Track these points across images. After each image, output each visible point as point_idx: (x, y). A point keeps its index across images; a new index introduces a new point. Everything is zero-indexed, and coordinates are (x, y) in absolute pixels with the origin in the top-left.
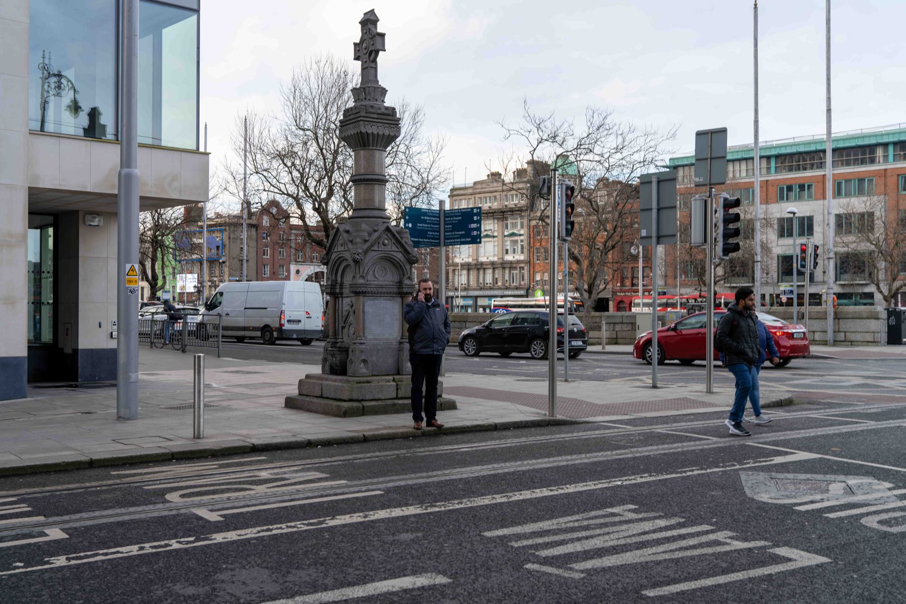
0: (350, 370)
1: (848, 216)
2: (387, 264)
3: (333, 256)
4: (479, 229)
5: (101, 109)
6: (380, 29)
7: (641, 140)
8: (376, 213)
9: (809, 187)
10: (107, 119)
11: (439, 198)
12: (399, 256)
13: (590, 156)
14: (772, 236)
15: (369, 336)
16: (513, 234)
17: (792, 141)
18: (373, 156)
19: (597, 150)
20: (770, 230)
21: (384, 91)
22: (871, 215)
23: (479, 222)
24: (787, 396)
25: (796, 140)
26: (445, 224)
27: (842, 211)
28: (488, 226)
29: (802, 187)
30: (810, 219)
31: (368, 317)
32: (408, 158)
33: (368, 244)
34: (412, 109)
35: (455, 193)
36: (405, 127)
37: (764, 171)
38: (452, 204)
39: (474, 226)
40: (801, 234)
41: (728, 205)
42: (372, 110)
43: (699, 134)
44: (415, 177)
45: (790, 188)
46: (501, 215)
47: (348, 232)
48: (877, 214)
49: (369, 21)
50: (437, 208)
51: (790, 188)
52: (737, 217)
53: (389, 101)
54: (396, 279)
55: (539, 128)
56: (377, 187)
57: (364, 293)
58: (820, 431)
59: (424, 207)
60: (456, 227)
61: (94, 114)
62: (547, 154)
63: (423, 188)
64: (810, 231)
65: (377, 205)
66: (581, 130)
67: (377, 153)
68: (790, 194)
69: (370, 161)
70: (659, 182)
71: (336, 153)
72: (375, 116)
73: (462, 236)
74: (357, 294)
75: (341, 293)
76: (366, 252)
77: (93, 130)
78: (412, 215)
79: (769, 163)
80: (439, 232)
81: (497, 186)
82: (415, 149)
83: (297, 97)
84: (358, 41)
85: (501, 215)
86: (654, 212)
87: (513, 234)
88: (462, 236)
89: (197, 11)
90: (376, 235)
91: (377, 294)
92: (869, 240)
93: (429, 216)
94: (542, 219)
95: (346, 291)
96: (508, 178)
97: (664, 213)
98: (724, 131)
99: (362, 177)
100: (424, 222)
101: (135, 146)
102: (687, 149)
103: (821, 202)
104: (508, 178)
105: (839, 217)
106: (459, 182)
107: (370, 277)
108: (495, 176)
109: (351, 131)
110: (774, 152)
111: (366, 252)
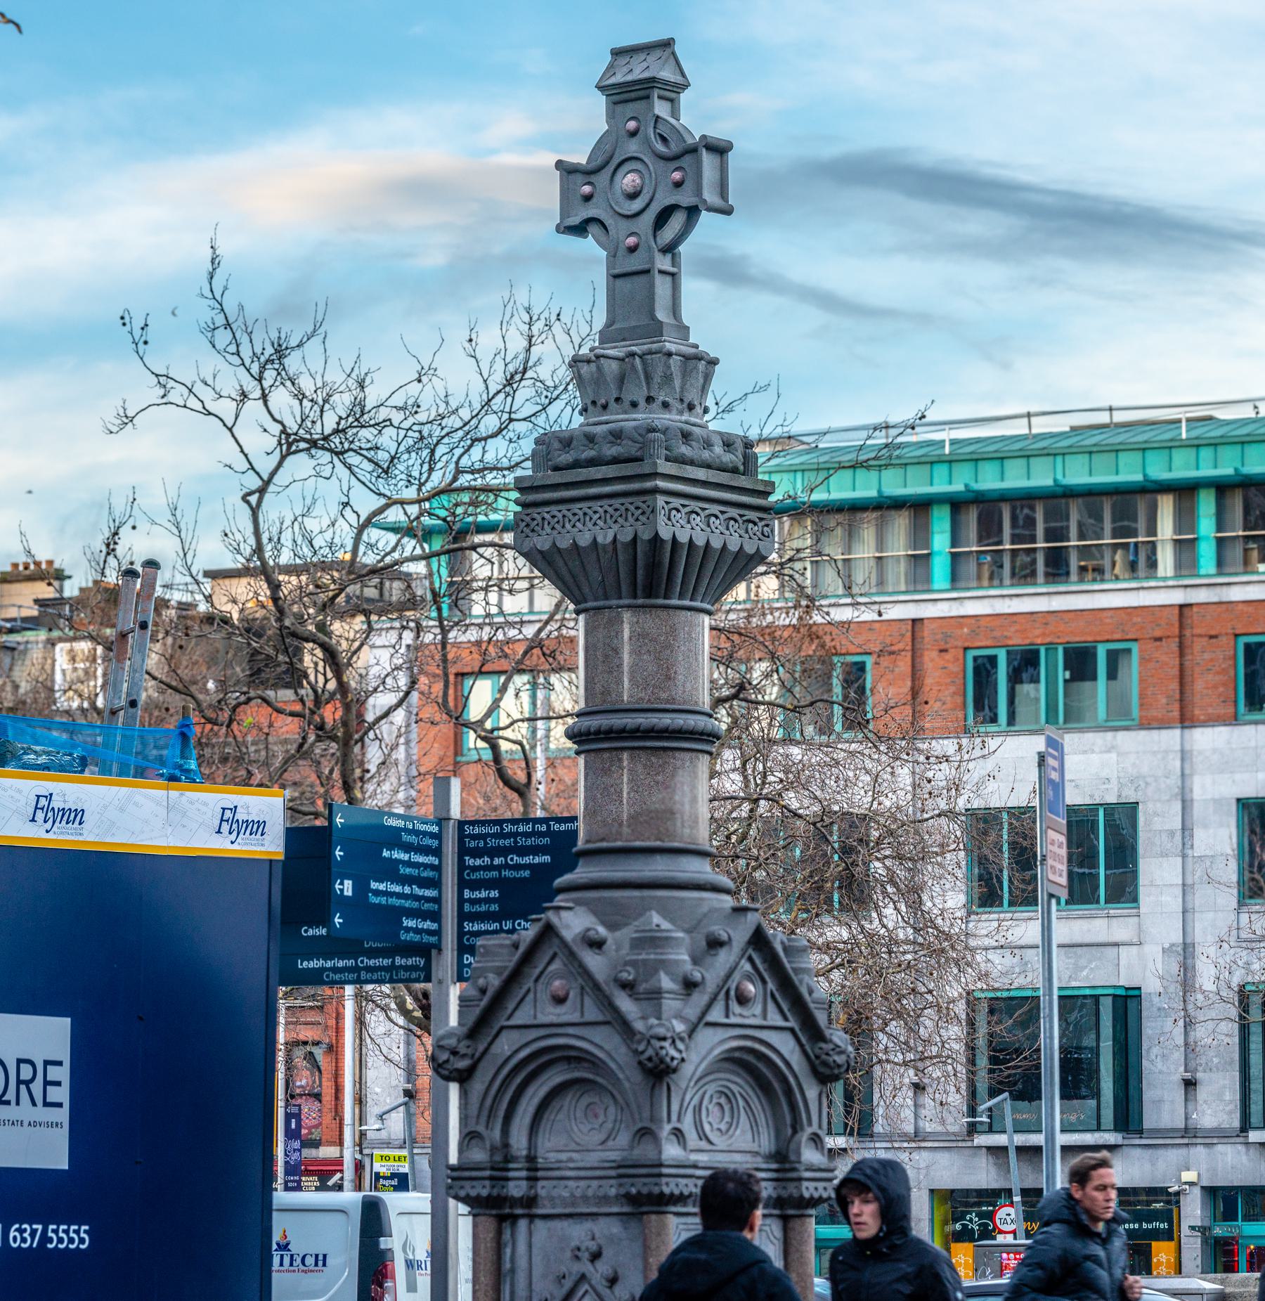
2: (739, 1084)
3: (506, 1045)
9: (1114, 659)
17: (1020, 428)
21: (701, 365)
25: (1041, 426)
26: (463, 884)
29: (1080, 663)
33: (700, 999)
37: (898, 574)
42: (684, 450)
49: (639, 85)
51: (1025, 664)
68: (1025, 689)
72: (701, 474)
75: (531, 1201)
80: (436, 916)
84: (580, 157)
93: (408, 848)
99: (618, 721)
100: (390, 871)
103: (1171, 737)
109: (595, 529)
110: (942, 483)
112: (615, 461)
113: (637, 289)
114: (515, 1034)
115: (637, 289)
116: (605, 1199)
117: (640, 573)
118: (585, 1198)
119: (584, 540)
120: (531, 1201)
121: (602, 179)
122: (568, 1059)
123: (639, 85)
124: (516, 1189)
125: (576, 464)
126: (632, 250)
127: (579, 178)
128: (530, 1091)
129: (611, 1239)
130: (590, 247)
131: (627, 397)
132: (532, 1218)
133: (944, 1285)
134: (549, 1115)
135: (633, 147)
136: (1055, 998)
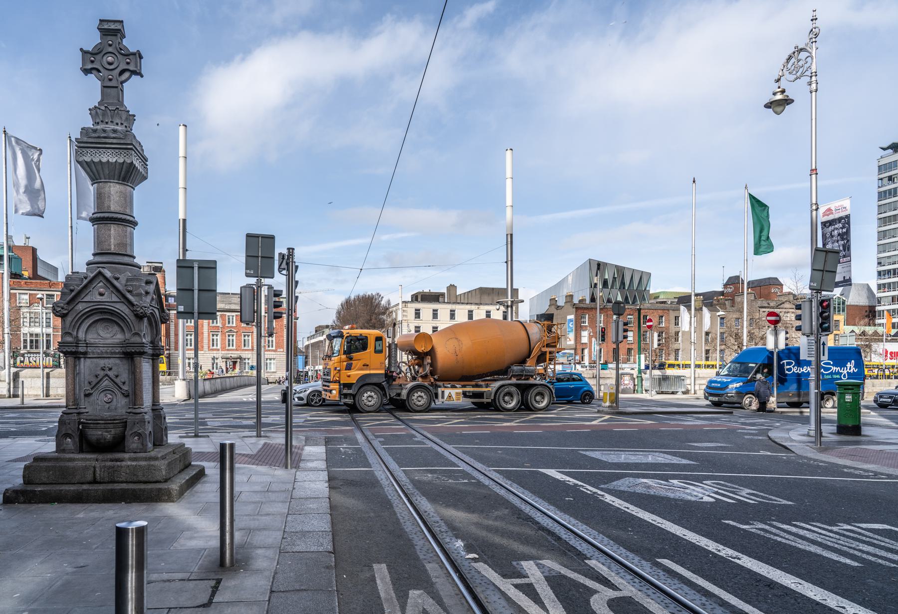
3: (80, 307)
8: (126, 260)
49: (111, 31)
86: (196, 292)
99: (111, 215)
112: (114, 138)
113: (112, 91)
114: (84, 304)
115: (112, 91)
116: (115, 353)
117: (123, 173)
118: (107, 353)
119: (104, 160)
120: (85, 353)
121: (98, 57)
122: (101, 313)
123: (111, 31)
124: (81, 350)
125: (99, 137)
126: (110, 80)
127: (89, 55)
128: (84, 325)
129: (116, 364)
130: (92, 77)
131: (115, 122)
132: (85, 358)
133: (576, 518)
134: (91, 329)
135: (110, 49)
136: (364, 332)
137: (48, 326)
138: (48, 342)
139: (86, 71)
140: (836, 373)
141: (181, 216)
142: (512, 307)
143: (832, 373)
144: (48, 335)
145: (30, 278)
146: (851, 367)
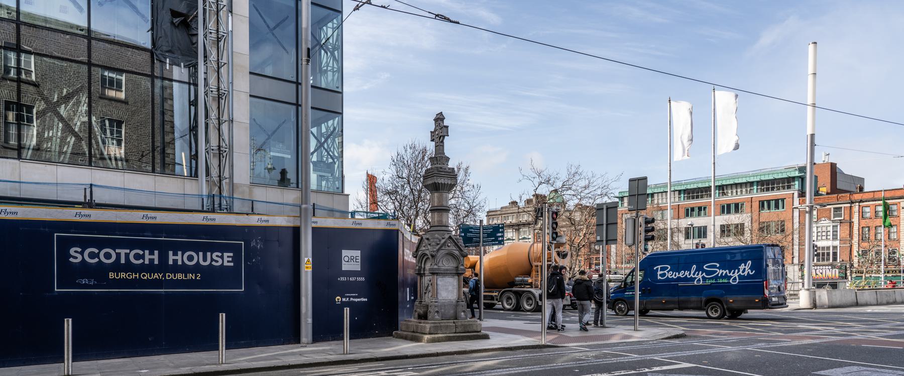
0: (430, 317)
1: (728, 226)
2: (450, 257)
4: (503, 236)
5: (287, 170)
6: (446, 123)
7: (600, 181)
8: (444, 228)
9: (705, 208)
10: (291, 175)
11: (482, 217)
12: (457, 253)
13: (569, 192)
14: (681, 238)
15: (440, 298)
16: (524, 238)
18: (442, 196)
19: (574, 188)
20: (680, 234)
21: (448, 159)
22: (742, 225)
23: (503, 232)
24: (682, 332)
27: (725, 223)
28: (509, 234)
29: (700, 209)
30: (705, 227)
31: (439, 287)
32: (462, 192)
34: (464, 166)
35: (490, 214)
36: (460, 178)
38: (488, 221)
39: (500, 234)
40: (699, 237)
41: (647, 222)
43: (631, 180)
44: (466, 205)
45: (693, 209)
46: (517, 227)
47: (428, 239)
48: (746, 224)
49: (439, 118)
50: (478, 224)
51: (693, 209)
52: (653, 229)
53: (451, 165)
54: (455, 265)
55: (539, 176)
56: (445, 214)
57: (437, 274)
58: (698, 352)
59: (472, 223)
60: (489, 235)
61: (283, 172)
62: (544, 190)
63: (470, 212)
64: (705, 236)
65: (444, 224)
66: (564, 177)
67: (444, 195)
69: (440, 199)
70: (607, 209)
71: (420, 191)
73: (493, 241)
74: (433, 274)
76: (438, 250)
77: (283, 181)
78: (465, 230)
79: (680, 194)
81: (515, 209)
82: (466, 189)
83: (398, 162)
85: (517, 227)
86: (605, 226)
87: (524, 238)
88: (493, 241)
89: (342, 114)
90: (443, 241)
91: (445, 274)
92: (740, 240)
94: (541, 229)
95: (427, 272)
96: (522, 204)
97: (610, 226)
98: (645, 178)
100: (471, 232)
101: (309, 191)
102: (625, 187)
104: (522, 204)
105: (722, 226)
106: (493, 207)
107: (440, 264)
108: (514, 203)
109: (430, 182)
110: (683, 188)
111: (438, 250)
137: (835, 238)
138: (835, 254)
139: (447, 127)
140: (722, 277)
141: (809, 132)
142: (811, 212)
143: (717, 278)
144: (835, 247)
145: (828, 194)
146: (746, 269)
